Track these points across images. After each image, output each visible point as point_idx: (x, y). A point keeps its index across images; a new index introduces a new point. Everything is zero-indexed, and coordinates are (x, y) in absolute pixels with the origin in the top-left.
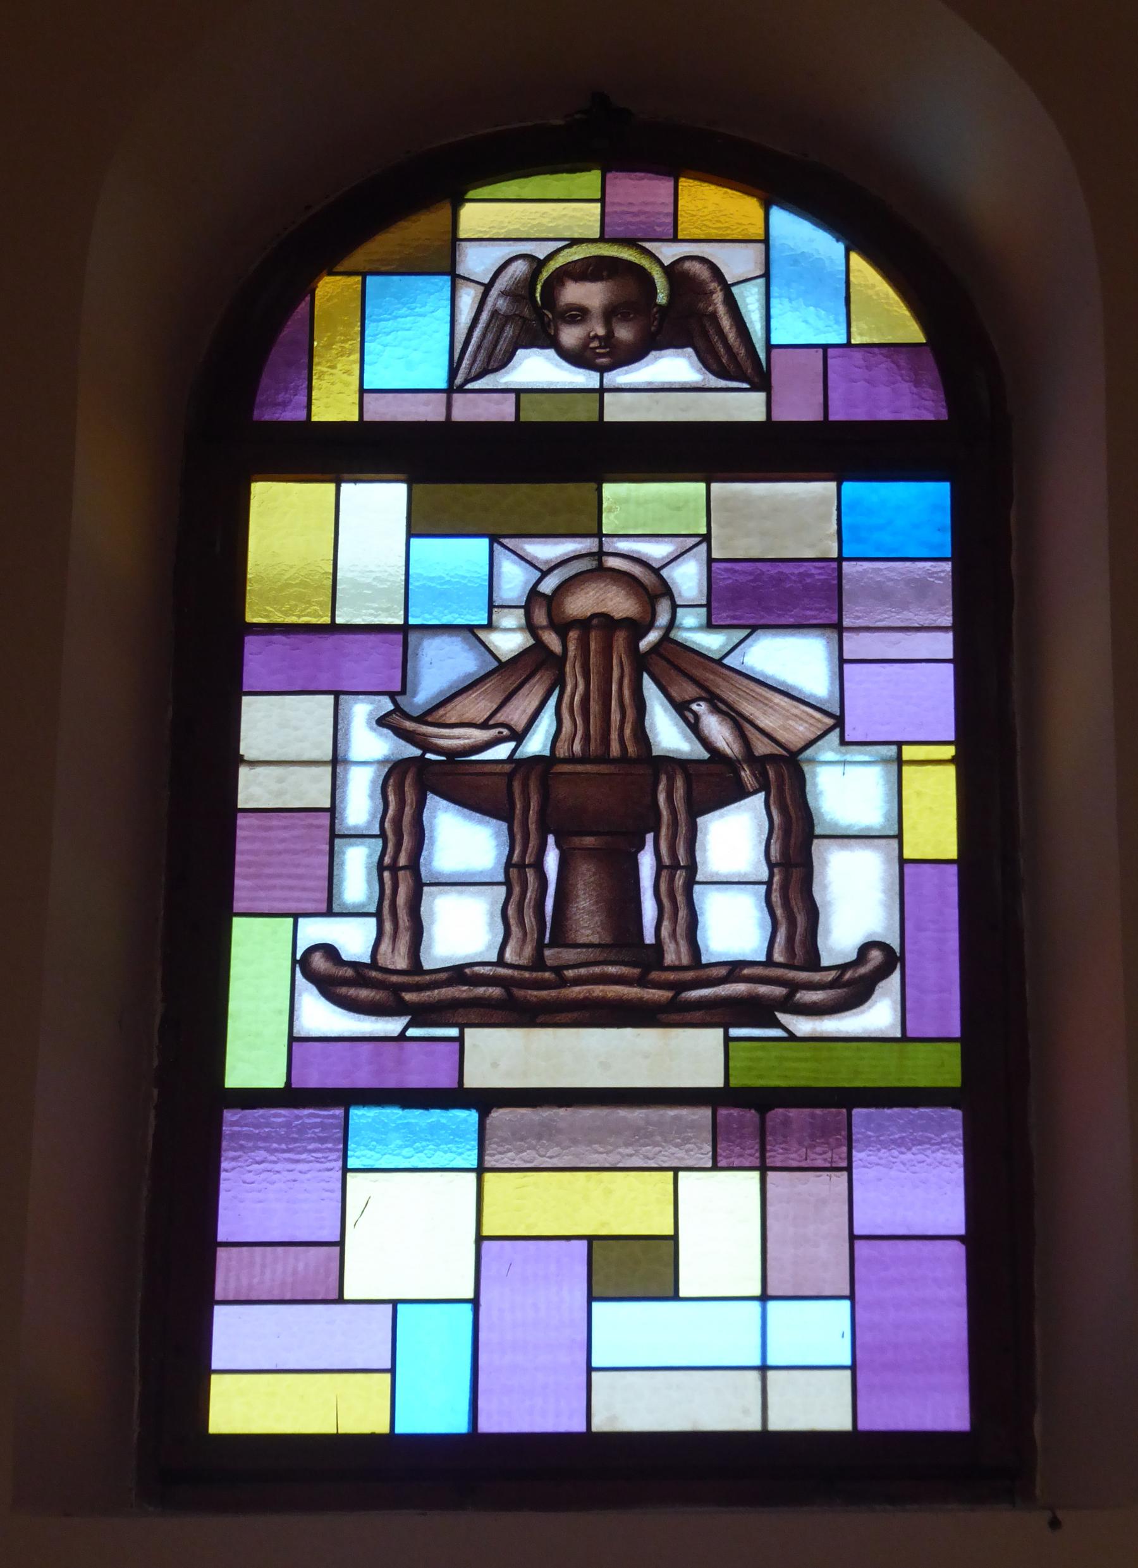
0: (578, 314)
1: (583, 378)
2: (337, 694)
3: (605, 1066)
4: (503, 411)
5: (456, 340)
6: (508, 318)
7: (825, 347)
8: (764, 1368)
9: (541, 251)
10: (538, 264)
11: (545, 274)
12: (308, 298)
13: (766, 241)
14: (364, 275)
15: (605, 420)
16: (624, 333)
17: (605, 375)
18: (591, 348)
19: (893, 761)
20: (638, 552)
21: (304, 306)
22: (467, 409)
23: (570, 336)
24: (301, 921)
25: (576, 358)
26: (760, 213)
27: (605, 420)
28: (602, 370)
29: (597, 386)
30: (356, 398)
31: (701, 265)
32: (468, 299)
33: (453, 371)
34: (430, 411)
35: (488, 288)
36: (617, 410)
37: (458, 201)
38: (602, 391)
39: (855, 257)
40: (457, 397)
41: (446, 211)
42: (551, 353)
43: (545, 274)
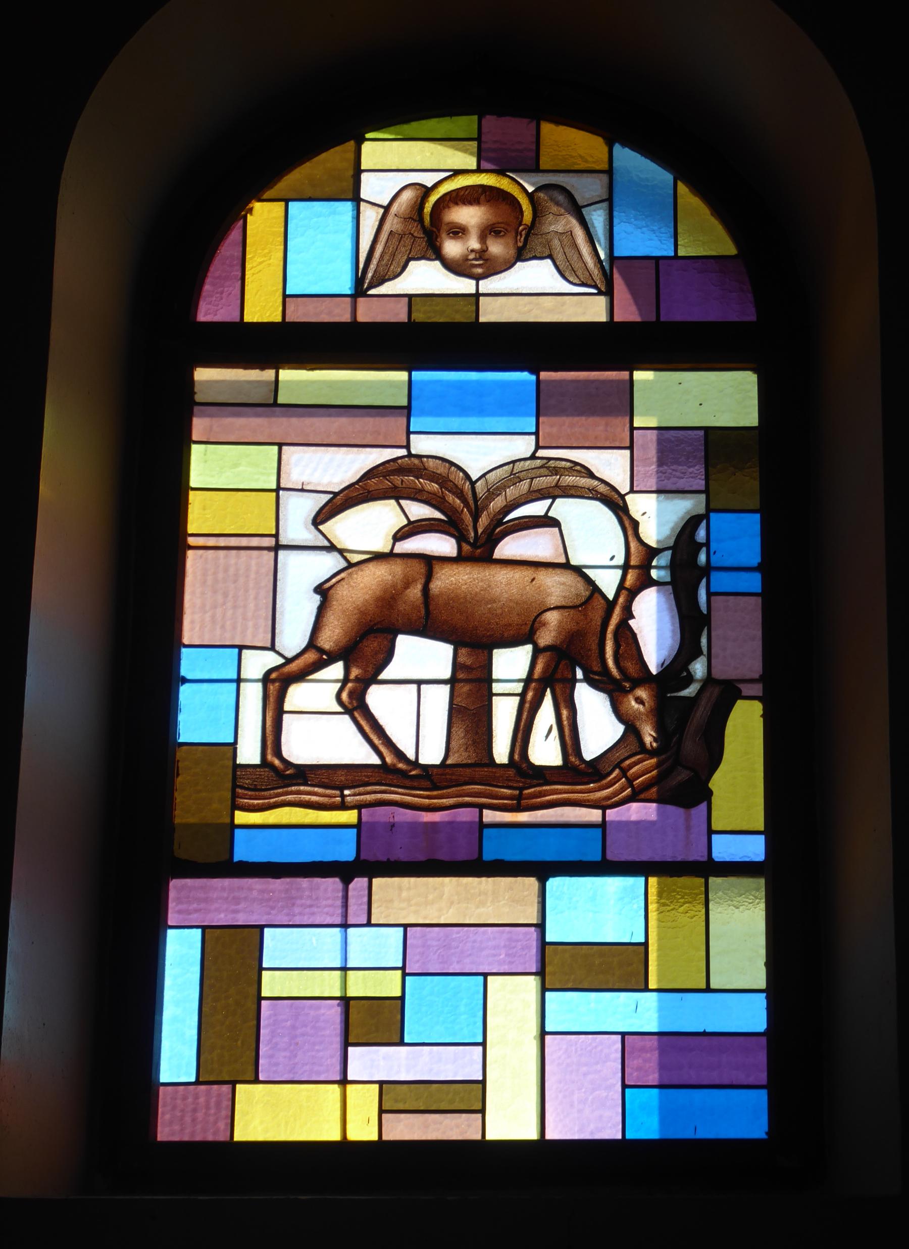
0: (459, 232)
1: (465, 286)
2: (280, 445)
3: (606, 745)
4: (398, 314)
5: (361, 251)
6: (402, 236)
7: (657, 259)
8: (344, 1082)
9: (429, 180)
10: (427, 191)
11: (433, 198)
12: (241, 222)
13: (610, 172)
14: (287, 201)
15: (480, 321)
16: (496, 248)
17: (481, 282)
18: (331, 660)
19: (346, 932)
20: (605, 235)
21: (235, 235)
22: (367, 313)
23: (452, 248)
24: (284, 448)
25: (455, 268)
26: (605, 149)
27: (480, 321)
28: (478, 278)
29: (473, 291)
30: (280, 299)
31: (352, 672)
32: (370, 218)
33: (359, 281)
34: (341, 314)
35: (387, 209)
36: (491, 312)
37: (361, 140)
38: (477, 295)
39: (680, 185)
40: (361, 301)
41: (351, 144)
42: (437, 263)
43: (433, 198)
